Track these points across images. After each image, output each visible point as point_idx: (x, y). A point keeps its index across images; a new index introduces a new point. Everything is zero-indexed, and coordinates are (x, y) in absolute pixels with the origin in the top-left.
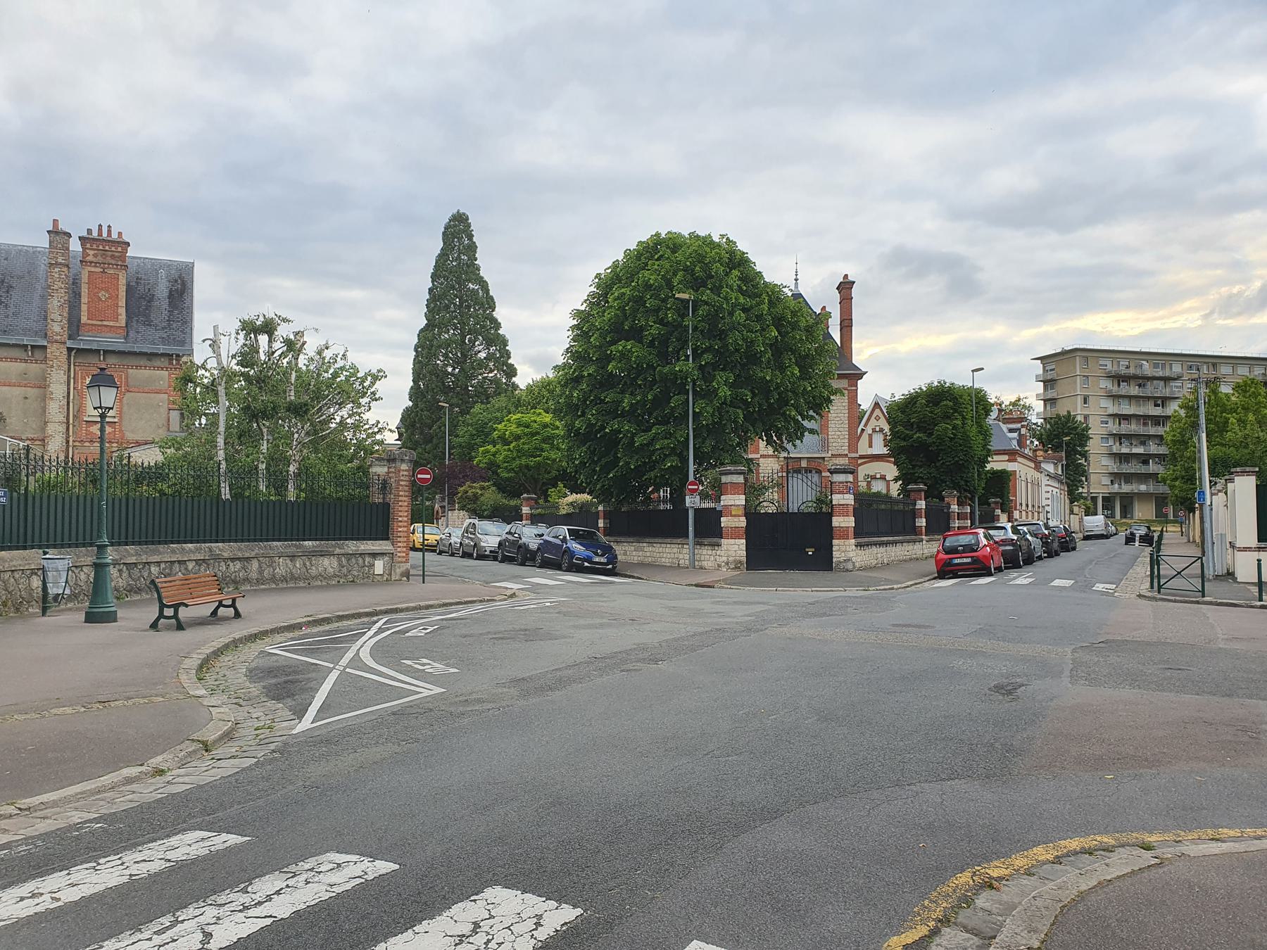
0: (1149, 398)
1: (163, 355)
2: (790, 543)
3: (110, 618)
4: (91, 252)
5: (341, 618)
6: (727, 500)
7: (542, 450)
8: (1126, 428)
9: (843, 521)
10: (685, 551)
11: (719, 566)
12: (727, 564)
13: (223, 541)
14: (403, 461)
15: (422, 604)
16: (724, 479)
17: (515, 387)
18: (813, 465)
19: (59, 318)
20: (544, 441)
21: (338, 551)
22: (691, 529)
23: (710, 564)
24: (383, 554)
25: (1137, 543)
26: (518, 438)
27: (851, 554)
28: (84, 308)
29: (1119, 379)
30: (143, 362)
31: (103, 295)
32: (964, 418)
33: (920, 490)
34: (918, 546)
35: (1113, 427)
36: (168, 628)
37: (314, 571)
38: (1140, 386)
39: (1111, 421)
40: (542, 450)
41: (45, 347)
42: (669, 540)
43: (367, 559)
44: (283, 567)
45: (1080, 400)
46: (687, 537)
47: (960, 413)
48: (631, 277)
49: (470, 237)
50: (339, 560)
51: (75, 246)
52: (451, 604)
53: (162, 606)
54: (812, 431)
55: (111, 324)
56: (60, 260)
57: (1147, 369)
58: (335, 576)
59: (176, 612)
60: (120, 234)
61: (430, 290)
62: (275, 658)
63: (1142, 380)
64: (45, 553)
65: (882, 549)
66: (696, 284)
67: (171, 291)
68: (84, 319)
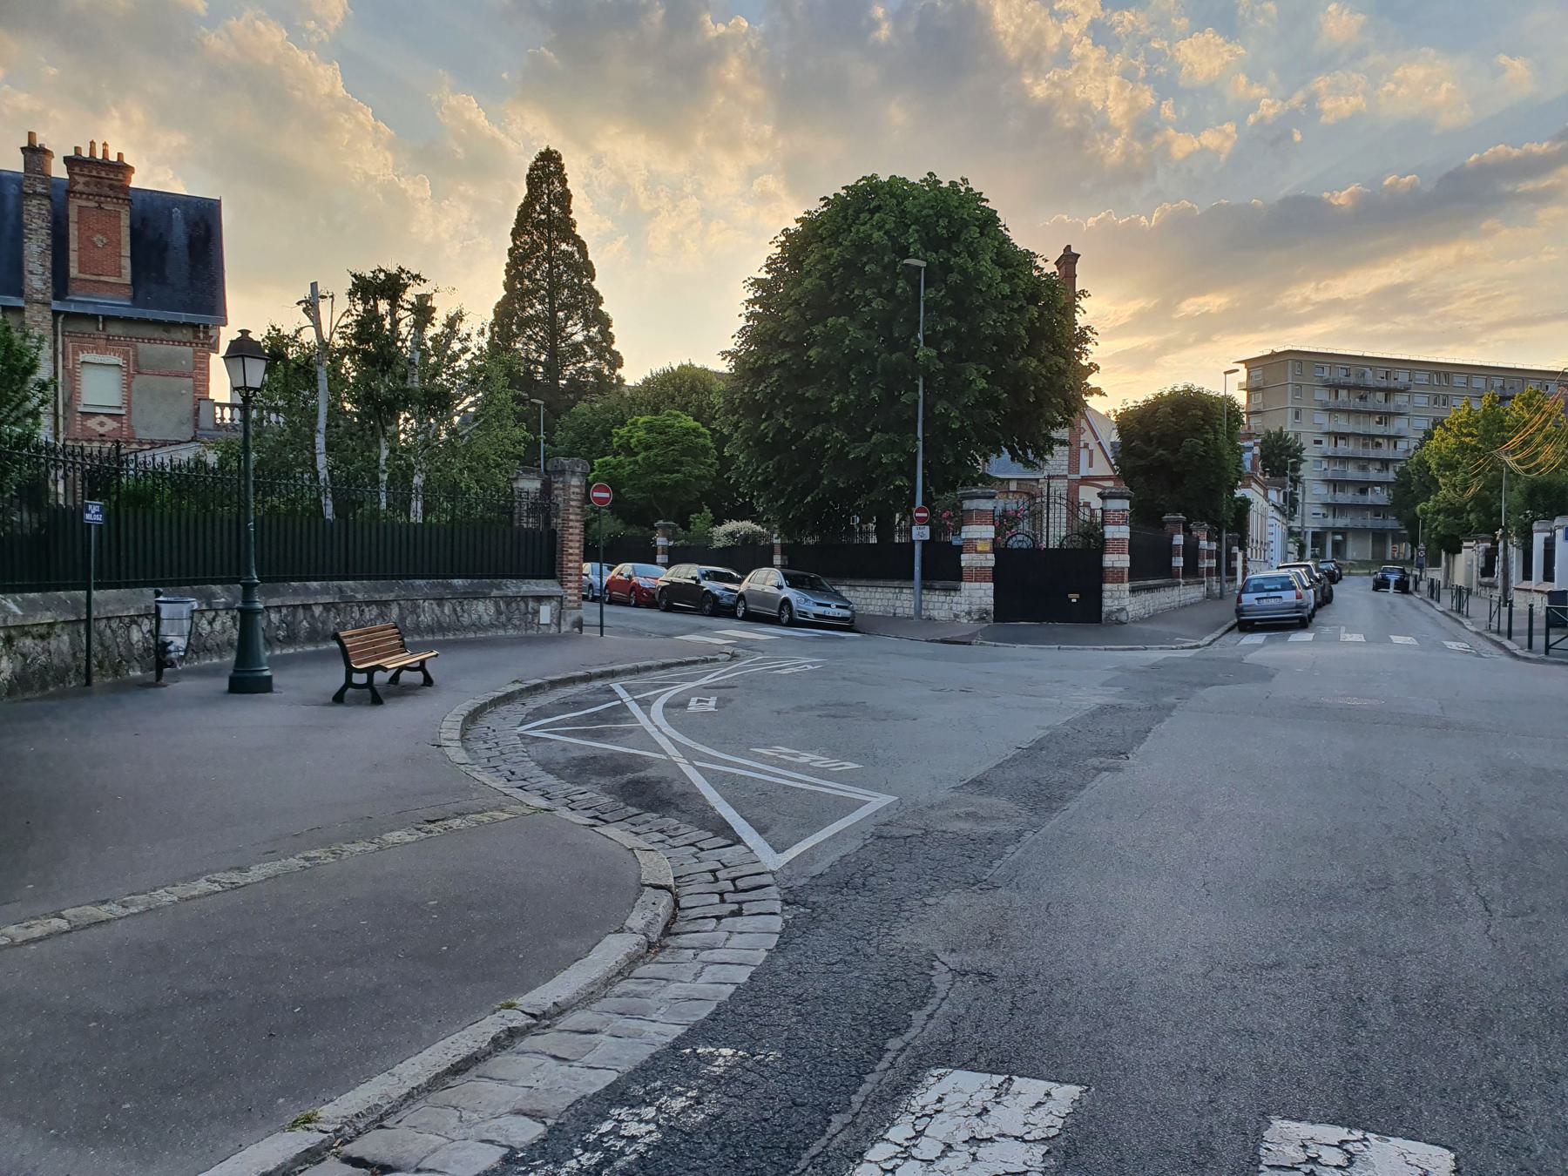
0: (1370, 413)
1: (185, 325)
2: (1048, 591)
3: (265, 686)
4: (81, 180)
5: (554, 684)
6: (971, 531)
7: (681, 464)
8: (1344, 448)
9: (1117, 560)
10: (904, 597)
11: (956, 616)
12: (969, 613)
13: (354, 579)
14: (573, 473)
15: (640, 664)
16: (967, 504)
17: (621, 380)
18: (1024, 488)
19: (41, 270)
20: (684, 453)
21: (495, 593)
22: (917, 568)
23: (943, 614)
24: (549, 598)
25: (1391, 590)
26: (648, 448)
27: (1126, 602)
28: (73, 256)
29: (1335, 387)
30: (158, 333)
31: (98, 239)
32: (1216, 432)
33: (1178, 521)
34: (1176, 591)
35: (1328, 447)
36: (358, 702)
37: (465, 620)
38: (1361, 398)
39: (1325, 440)
40: (681, 464)
41: (20, 310)
42: (881, 583)
43: (531, 604)
44: (428, 612)
45: (1290, 414)
46: (911, 578)
47: (1213, 427)
48: (834, 238)
49: (564, 181)
50: (497, 606)
51: (58, 170)
52: (695, 662)
53: (350, 671)
54: (1063, 443)
55: (112, 280)
56: (39, 189)
57: (1371, 379)
58: (492, 625)
59: (370, 678)
60: (120, 155)
61: (511, 252)
62: (541, 746)
63: (1363, 390)
64: (158, 594)
65: (1149, 596)
66: (932, 243)
67: (191, 237)
68: (74, 272)
